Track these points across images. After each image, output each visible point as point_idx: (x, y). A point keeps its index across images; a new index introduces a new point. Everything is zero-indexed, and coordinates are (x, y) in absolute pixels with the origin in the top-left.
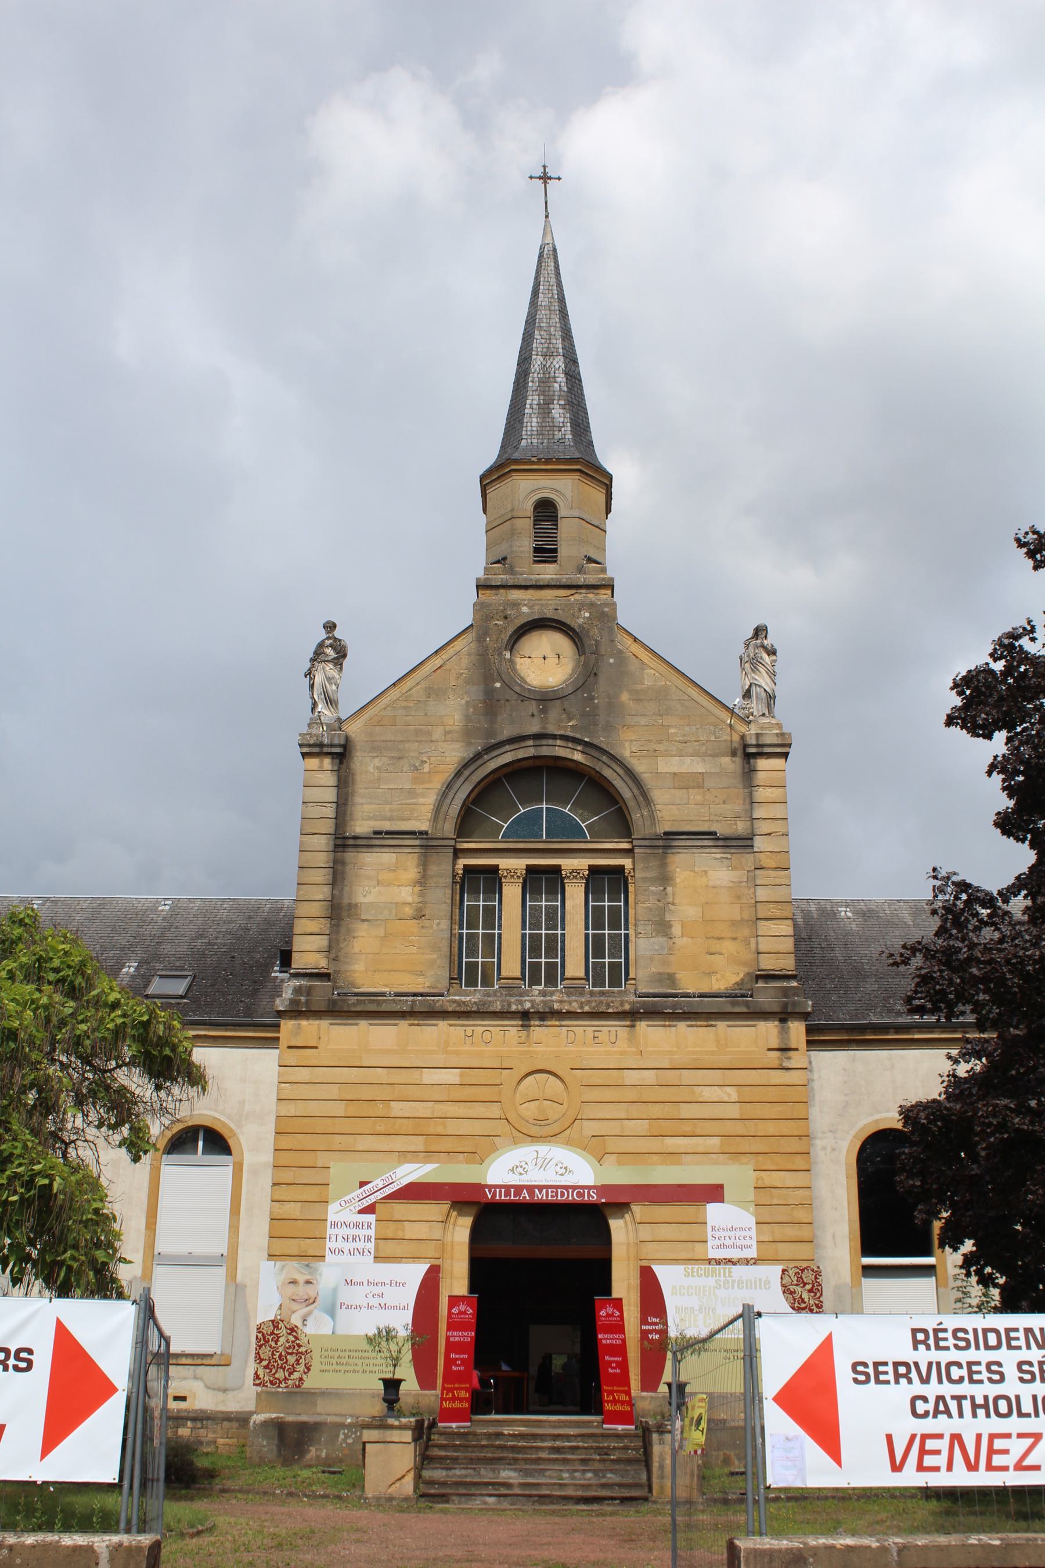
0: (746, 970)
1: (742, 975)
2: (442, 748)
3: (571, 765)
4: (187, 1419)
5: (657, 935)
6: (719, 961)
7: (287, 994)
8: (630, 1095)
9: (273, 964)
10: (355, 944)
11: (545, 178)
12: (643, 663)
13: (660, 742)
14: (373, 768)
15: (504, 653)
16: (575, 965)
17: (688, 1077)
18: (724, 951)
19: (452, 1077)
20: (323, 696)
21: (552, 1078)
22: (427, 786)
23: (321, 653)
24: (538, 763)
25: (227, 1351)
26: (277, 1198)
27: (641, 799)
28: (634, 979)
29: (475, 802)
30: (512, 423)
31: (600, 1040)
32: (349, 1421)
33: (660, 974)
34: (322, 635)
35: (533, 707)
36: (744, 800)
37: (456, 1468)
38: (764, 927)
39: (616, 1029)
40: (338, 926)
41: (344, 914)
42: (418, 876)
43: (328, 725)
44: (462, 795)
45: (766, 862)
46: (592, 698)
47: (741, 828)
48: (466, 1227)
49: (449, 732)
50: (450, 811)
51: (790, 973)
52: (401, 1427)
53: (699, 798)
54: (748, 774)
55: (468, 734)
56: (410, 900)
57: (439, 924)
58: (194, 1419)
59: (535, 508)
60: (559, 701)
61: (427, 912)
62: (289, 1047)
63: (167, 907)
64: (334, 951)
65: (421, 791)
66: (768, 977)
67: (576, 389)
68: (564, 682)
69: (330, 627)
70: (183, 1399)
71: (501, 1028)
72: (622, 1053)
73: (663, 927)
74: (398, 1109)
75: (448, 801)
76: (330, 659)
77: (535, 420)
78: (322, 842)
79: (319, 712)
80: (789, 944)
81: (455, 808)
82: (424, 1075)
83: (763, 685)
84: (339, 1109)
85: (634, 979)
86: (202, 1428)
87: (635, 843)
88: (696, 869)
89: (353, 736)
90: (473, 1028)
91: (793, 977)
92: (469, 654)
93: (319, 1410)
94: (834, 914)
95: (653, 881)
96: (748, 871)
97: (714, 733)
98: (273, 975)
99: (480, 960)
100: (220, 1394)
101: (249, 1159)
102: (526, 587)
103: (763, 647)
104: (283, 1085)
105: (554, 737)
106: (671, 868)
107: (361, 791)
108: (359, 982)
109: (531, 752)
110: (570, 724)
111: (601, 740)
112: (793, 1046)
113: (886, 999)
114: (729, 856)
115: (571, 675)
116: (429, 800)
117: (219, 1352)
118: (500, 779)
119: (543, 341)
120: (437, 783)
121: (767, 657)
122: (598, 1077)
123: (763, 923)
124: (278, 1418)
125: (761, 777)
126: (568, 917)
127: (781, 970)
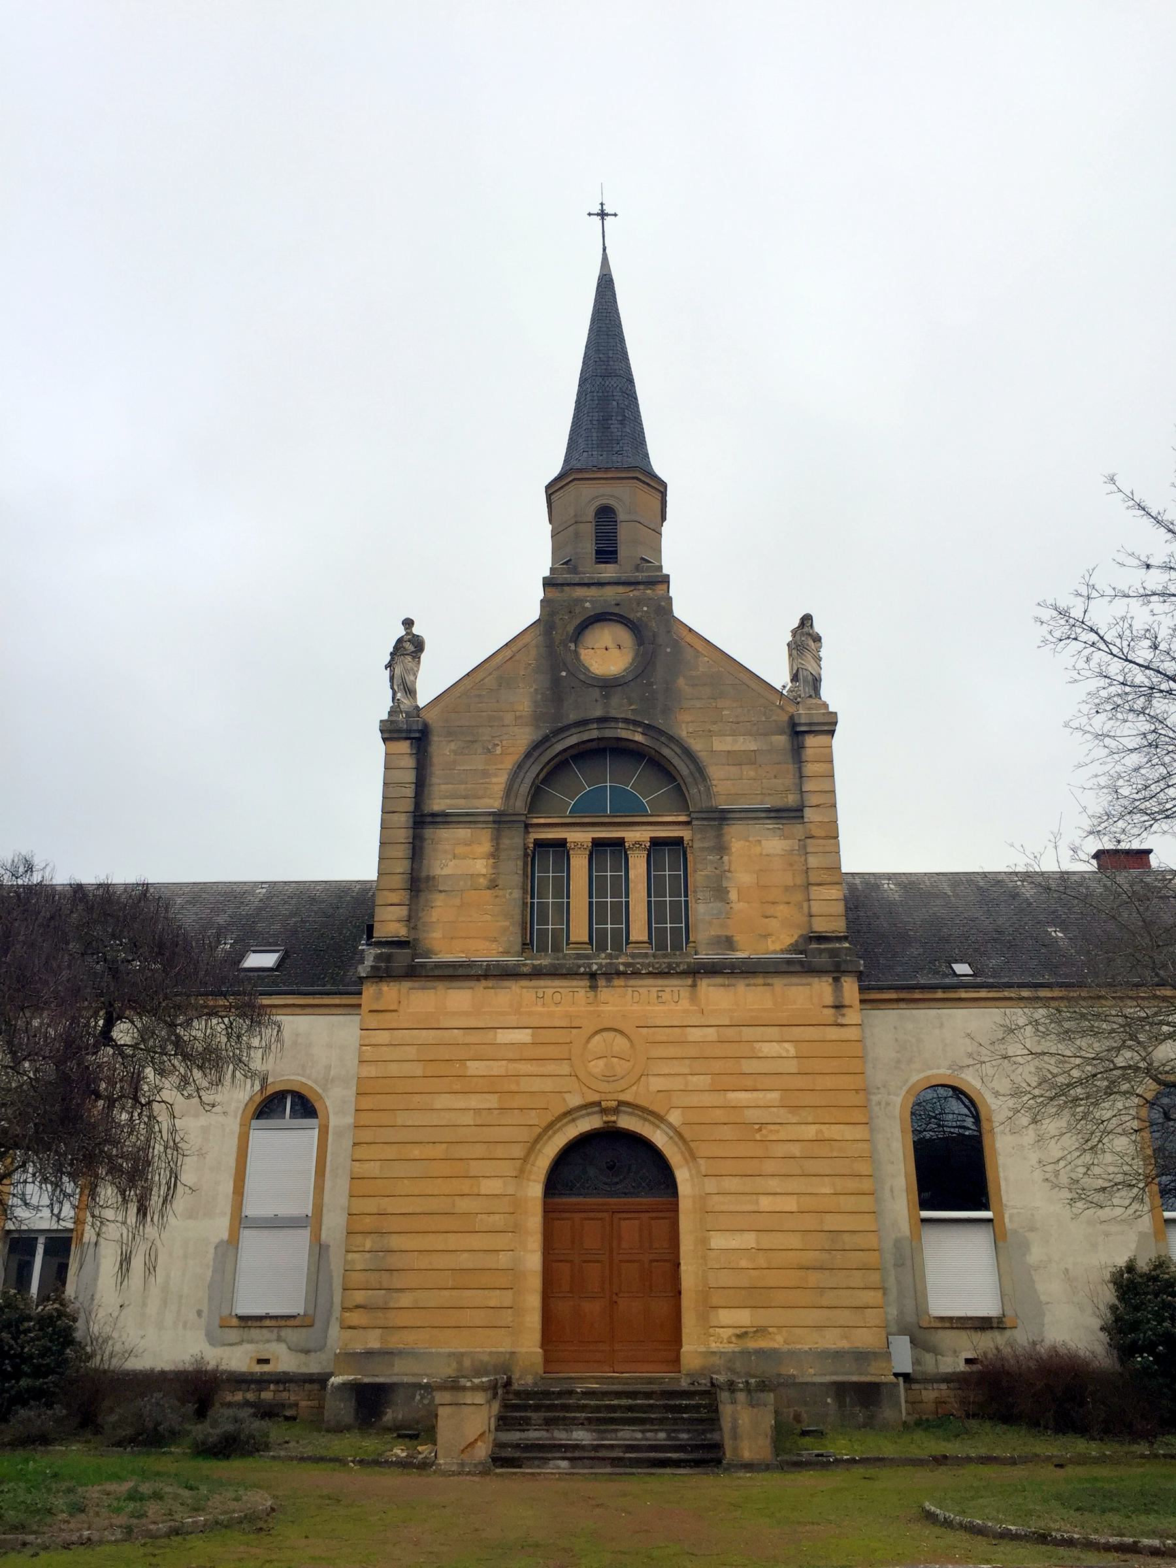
0: (800, 932)
1: (796, 937)
2: (513, 732)
3: (632, 746)
4: (270, 1382)
5: (715, 901)
6: (774, 924)
7: (369, 962)
8: (692, 1051)
9: (361, 938)
10: (434, 914)
11: (603, 215)
12: (698, 651)
13: (715, 723)
14: (449, 752)
15: (570, 644)
16: (639, 931)
17: (748, 1033)
18: (779, 914)
19: (524, 1036)
20: (402, 687)
21: (619, 1036)
22: (500, 767)
23: (400, 648)
24: (602, 745)
25: (311, 1312)
26: (357, 1157)
27: (697, 775)
28: (694, 942)
29: (545, 781)
30: (575, 438)
31: (664, 999)
32: (425, 1381)
33: (719, 937)
34: (401, 632)
35: (596, 693)
36: (794, 775)
37: (528, 1430)
38: (815, 892)
39: (679, 988)
40: (417, 897)
41: (423, 886)
42: (492, 850)
43: (407, 713)
44: (531, 775)
45: (815, 831)
46: (651, 684)
47: (791, 800)
48: (539, 1182)
49: (520, 717)
50: (521, 789)
51: (842, 934)
52: (475, 1388)
53: (752, 774)
54: (797, 751)
55: (537, 719)
56: (484, 871)
57: (511, 893)
58: (277, 1382)
59: (596, 514)
60: (620, 687)
61: (500, 882)
62: (370, 1011)
63: (264, 890)
64: (413, 920)
65: (494, 771)
66: (821, 939)
67: (632, 406)
68: (625, 670)
69: (408, 623)
70: (267, 1361)
71: (571, 990)
72: (686, 1011)
73: (720, 893)
74: (474, 1067)
75: (519, 780)
76: (408, 652)
77: (595, 434)
78: (402, 820)
79: (398, 700)
80: (840, 908)
81: (525, 788)
82: (499, 1036)
83: (810, 669)
84: (418, 1069)
85: (694, 942)
86: (284, 1391)
87: (693, 815)
88: (751, 839)
89: (430, 722)
90: (544, 990)
91: (845, 938)
92: (537, 646)
93: (396, 1369)
94: (877, 887)
95: (710, 850)
96: (799, 840)
97: (765, 714)
98: (360, 948)
99: (550, 927)
100: (302, 1356)
101: (333, 1121)
102: (588, 585)
103: (809, 634)
104: (364, 1048)
105: (616, 720)
106: (727, 838)
107: (437, 772)
108: (437, 948)
109: (595, 734)
110: (632, 708)
111: (660, 723)
112: (847, 1004)
113: (932, 962)
114: (781, 826)
115: (634, 660)
116: (500, 781)
117: (302, 1313)
118: (567, 760)
119: (602, 363)
120: (509, 763)
121: (813, 644)
122: (661, 1034)
123: (815, 888)
124: (355, 1379)
125: (809, 753)
126: (631, 885)
127: (833, 932)
